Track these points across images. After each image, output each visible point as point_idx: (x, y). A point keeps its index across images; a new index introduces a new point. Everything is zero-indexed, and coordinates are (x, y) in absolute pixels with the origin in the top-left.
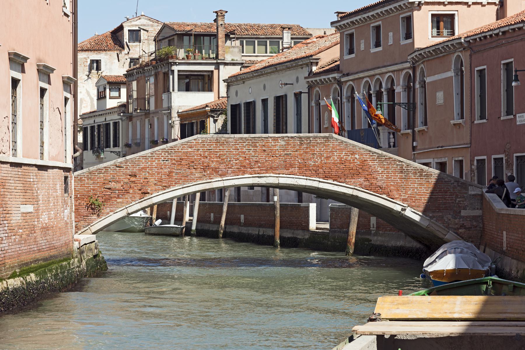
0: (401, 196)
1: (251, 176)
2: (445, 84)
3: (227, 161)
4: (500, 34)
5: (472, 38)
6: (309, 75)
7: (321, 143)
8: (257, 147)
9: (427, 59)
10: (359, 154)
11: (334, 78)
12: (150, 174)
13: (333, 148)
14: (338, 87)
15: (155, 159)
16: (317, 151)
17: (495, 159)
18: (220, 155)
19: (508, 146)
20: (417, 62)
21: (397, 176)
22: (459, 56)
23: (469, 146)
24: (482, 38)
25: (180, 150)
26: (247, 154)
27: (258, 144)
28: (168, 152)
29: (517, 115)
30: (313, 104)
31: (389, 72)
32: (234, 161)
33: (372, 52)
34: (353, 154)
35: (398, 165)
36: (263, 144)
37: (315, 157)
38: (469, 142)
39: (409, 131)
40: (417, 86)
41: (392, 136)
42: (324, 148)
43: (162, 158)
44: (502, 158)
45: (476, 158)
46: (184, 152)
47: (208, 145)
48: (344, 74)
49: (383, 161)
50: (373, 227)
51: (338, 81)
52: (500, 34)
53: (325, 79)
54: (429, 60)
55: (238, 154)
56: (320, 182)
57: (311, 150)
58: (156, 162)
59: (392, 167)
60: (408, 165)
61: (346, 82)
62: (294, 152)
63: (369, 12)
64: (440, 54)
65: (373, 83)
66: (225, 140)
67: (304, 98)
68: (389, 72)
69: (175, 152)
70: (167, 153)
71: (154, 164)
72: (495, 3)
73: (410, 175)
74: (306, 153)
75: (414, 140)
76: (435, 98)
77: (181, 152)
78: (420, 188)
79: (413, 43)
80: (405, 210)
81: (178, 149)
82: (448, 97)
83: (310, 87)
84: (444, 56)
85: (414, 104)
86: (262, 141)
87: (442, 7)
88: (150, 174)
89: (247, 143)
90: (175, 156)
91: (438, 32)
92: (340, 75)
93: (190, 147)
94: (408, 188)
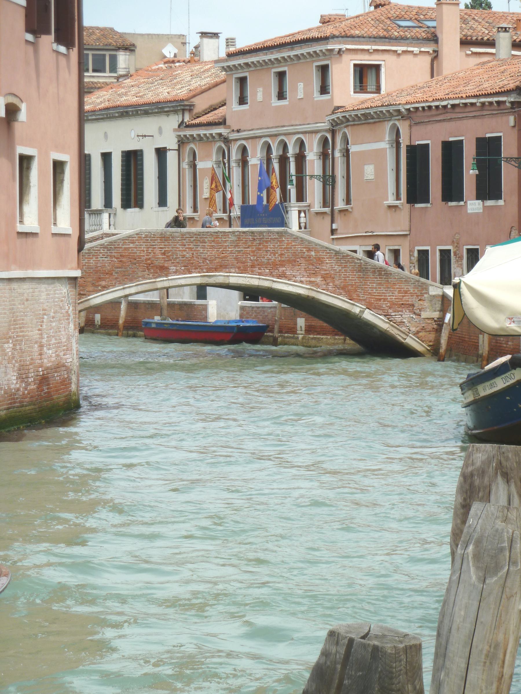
0: (360, 297)
1: (199, 275)
2: (376, 156)
3: (173, 258)
4: (449, 106)
5: (413, 106)
6: (179, 126)
7: (275, 238)
8: (205, 243)
9: (352, 123)
10: (315, 250)
11: (220, 135)
12: (88, 273)
13: (288, 244)
14: (223, 146)
15: (93, 255)
16: (270, 248)
17: (441, 251)
18: (165, 251)
19: (457, 237)
20: (337, 124)
21: (199, 245)
22: (394, 125)
23: (408, 233)
24: (426, 108)
25: (121, 246)
26: (195, 251)
27: (206, 240)
28: (108, 248)
29: (469, 202)
30: (185, 165)
31: (298, 133)
32: (181, 259)
33: (273, 105)
34: (309, 250)
35: (356, 263)
36: (213, 239)
37: (269, 254)
38: (408, 228)
39: (327, 210)
40: (337, 154)
41: (303, 215)
42: (279, 244)
43: (101, 255)
44: (450, 250)
45: (417, 248)
46: (125, 248)
47: (151, 240)
48: (233, 131)
49: (341, 258)
50: (301, 331)
51: (225, 138)
52: (449, 106)
53: (205, 135)
54: (354, 125)
55: (186, 251)
56: (273, 281)
57: (264, 246)
58: (94, 259)
59: (350, 265)
60: (366, 264)
61: (236, 140)
62: (246, 248)
63: (272, 53)
64: (370, 119)
65: (276, 145)
66: (171, 235)
67: (172, 158)
68: (298, 133)
69: (115, 248)
70: (106, 250)
71: (92, 261)
72: (428, 52)
73: (369, 274)
74: (259, 249)
75: (332, 222)
76: (362, 172)
77: (121, 248)
78: (379, 288)
79: (332, 100)
80: (363, 312)
81: (119, 245)
82: (380, 172)
83: (182, 142)
84: (375, 123)
85: (333, 177)
86: (211, 236)
87: (367, 57)
88: (88, 273)
89: (194, 239)
90: (115, 253)
91: (360, 86)
92: (228, 131)
93: (132, 243)
94: (367, 288)
